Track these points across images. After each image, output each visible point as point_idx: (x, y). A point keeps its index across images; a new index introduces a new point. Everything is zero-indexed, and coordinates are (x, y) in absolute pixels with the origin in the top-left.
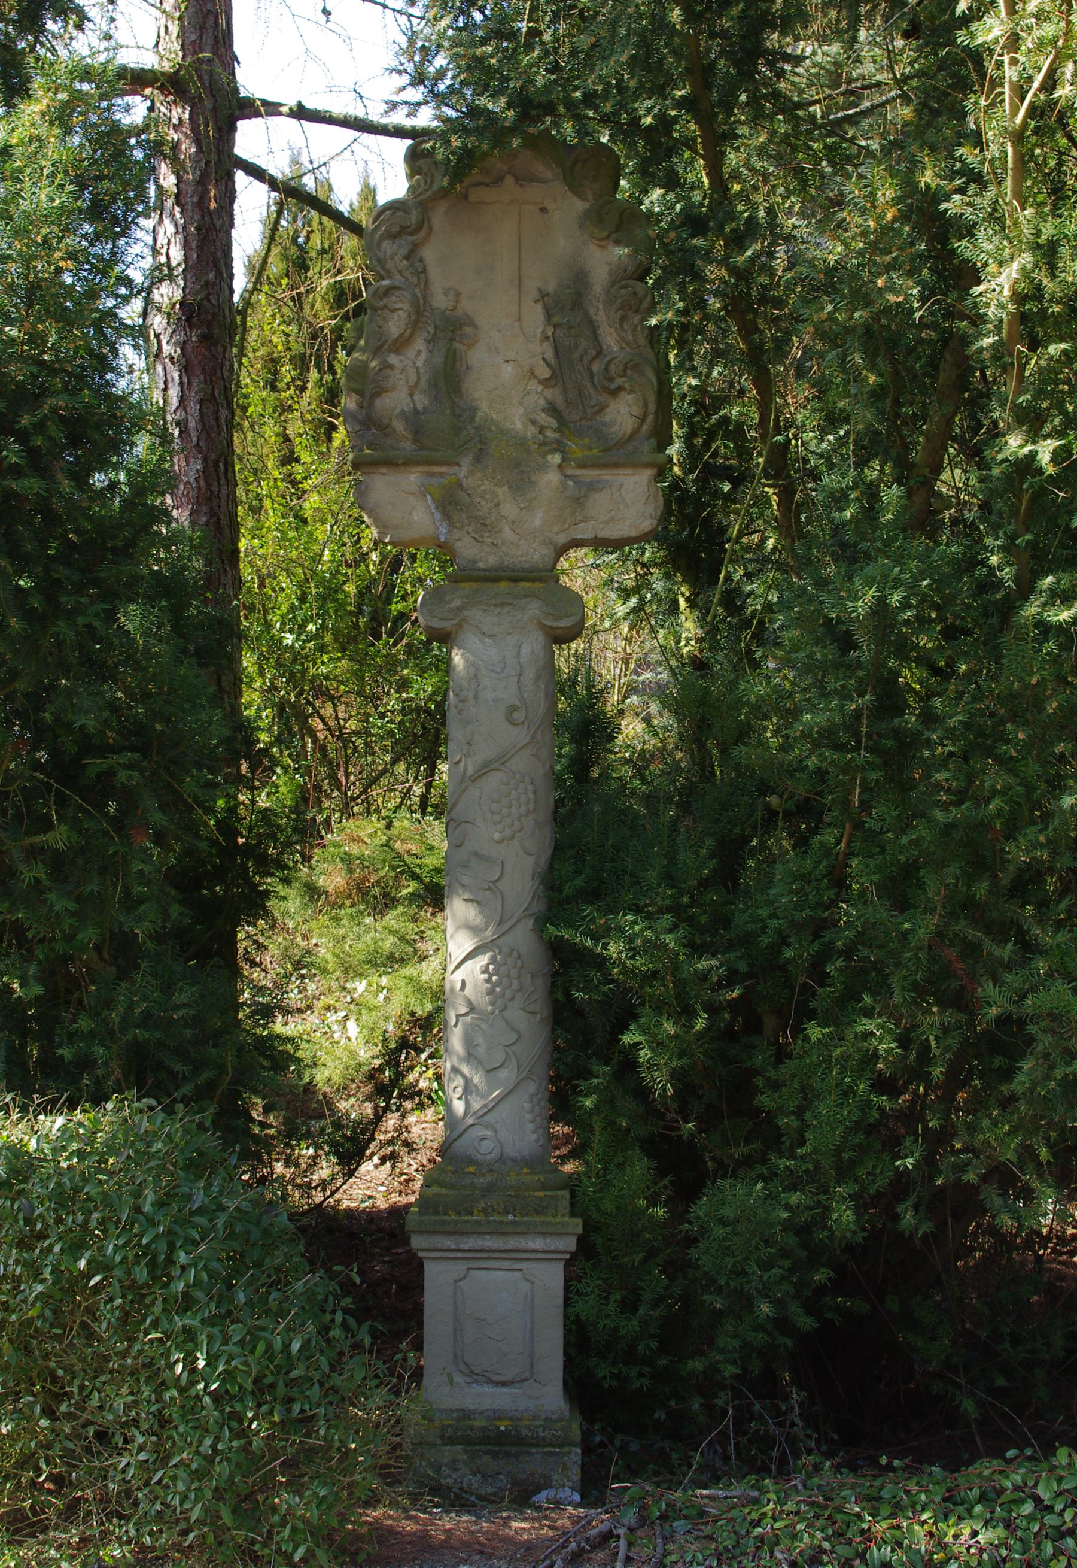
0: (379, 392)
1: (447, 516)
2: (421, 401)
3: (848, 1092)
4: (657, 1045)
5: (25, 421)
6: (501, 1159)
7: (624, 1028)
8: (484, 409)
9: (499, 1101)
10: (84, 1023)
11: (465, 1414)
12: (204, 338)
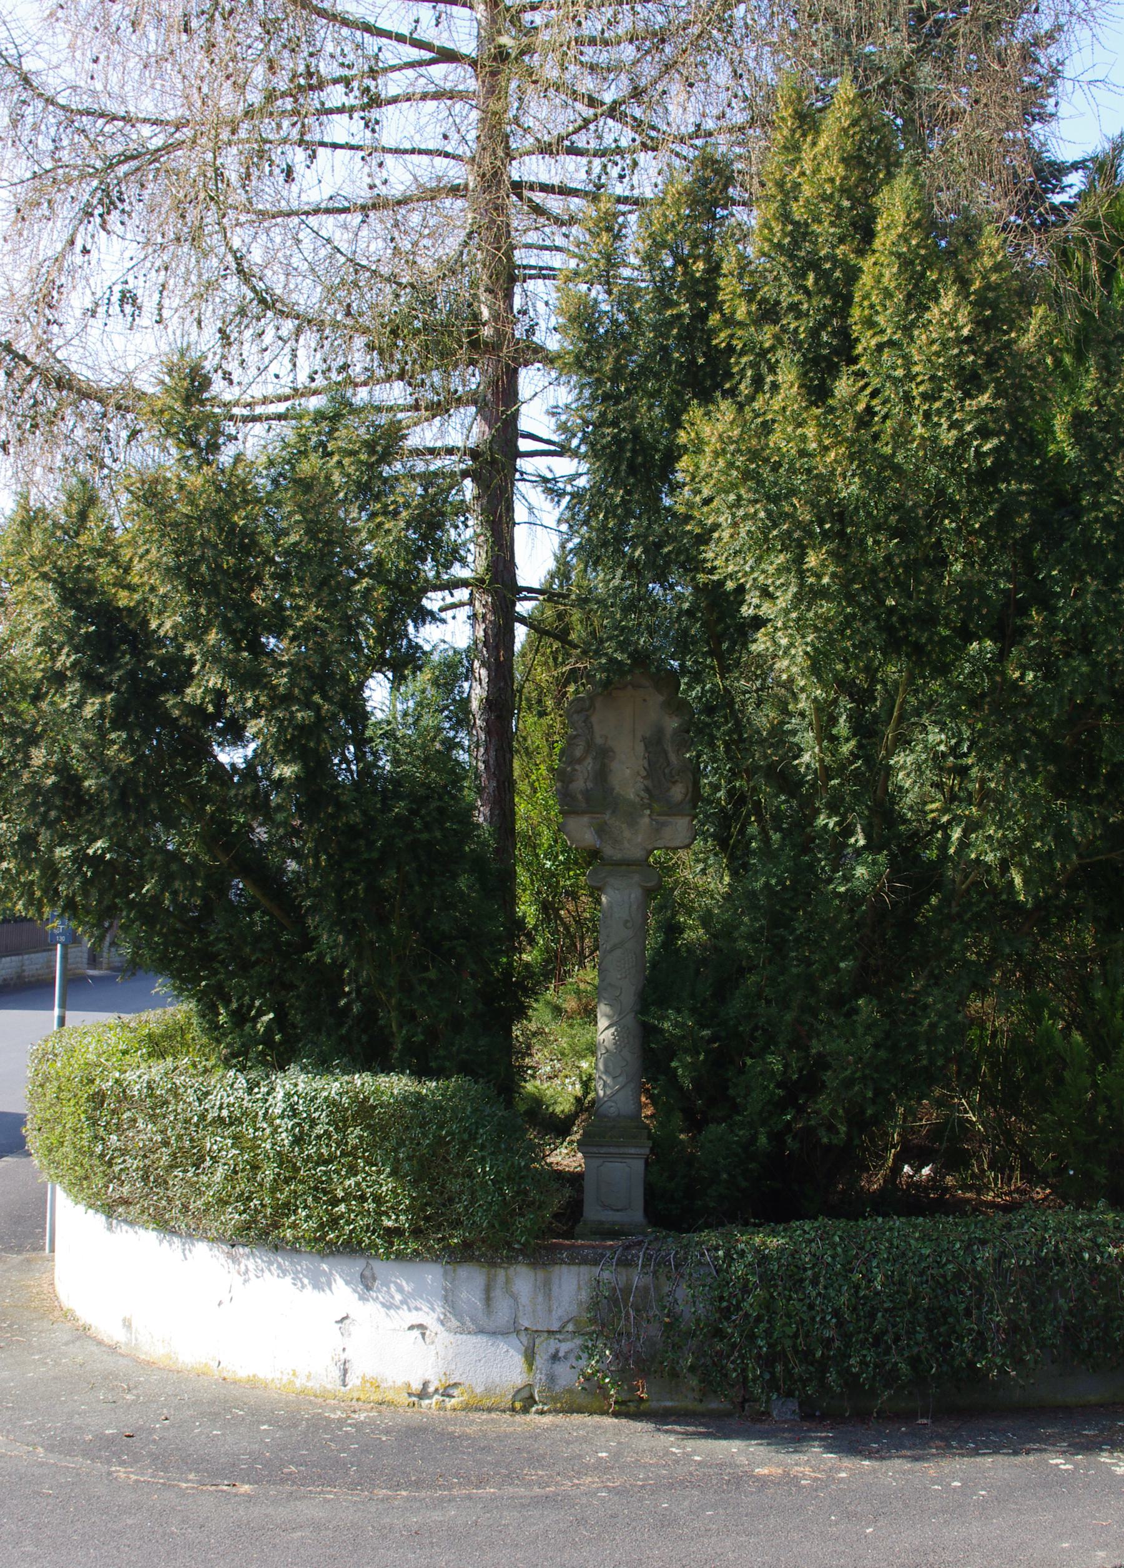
0: (571, 781)
1: (600, 837)
2: (590, 785)
3: (767, 1087)
4: (685, 1066)
5: (423, 812)
6: (619, 1116)
7: (672, 1060)
8: (617, 789)
9: (618, 1091)
10: (442, 1052)
11: (601, 1223)
12: (498, 717)
